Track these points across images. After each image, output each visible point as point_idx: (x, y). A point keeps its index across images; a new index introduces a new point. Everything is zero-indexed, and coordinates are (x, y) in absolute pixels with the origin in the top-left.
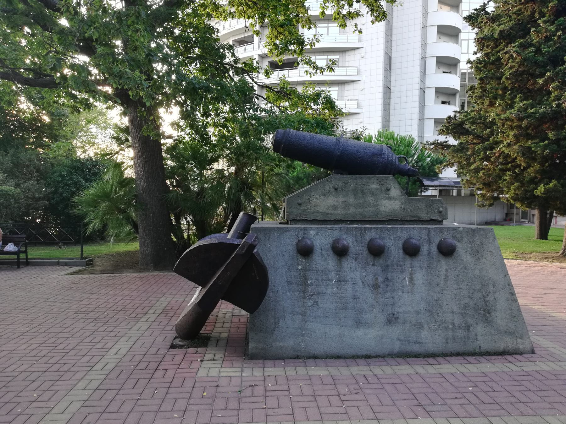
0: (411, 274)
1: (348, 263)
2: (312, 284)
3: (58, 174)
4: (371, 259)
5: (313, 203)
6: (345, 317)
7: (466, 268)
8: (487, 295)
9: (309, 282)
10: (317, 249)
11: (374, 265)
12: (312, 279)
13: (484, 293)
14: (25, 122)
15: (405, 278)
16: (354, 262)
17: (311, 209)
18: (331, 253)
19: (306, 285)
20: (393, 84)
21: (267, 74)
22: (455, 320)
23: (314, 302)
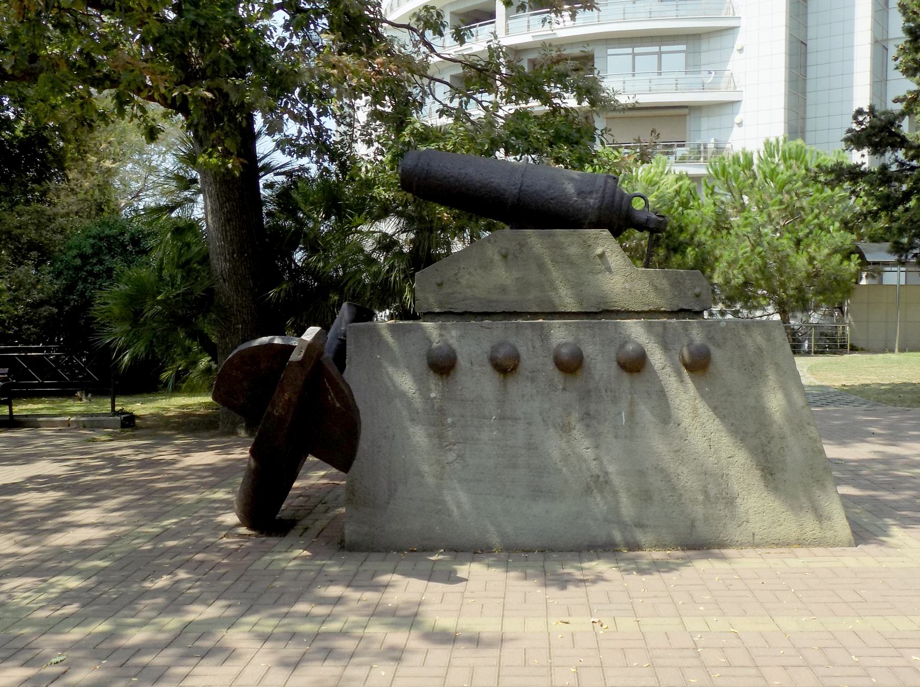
0: (632, 404)
1: (518, 387)
2: (453, 425)
3: (75, 252)
4: (558, 377)
5: (463, 282)
6: (512, 482)
7: (730, 395)
8: (769, 442)
9: (449, 420)
10: (462, 361)
11: (564, 389)
12: (453, 416)
13: (763, 438)
14: (11, 145)
15: (620, 413)
16: (529, 384)
17: (460, 293)
18: (489, 368)
19: (443, 425)
20: (811, 33)
21: (460, 37)
22: (709, 486)
23: (458, 456)
